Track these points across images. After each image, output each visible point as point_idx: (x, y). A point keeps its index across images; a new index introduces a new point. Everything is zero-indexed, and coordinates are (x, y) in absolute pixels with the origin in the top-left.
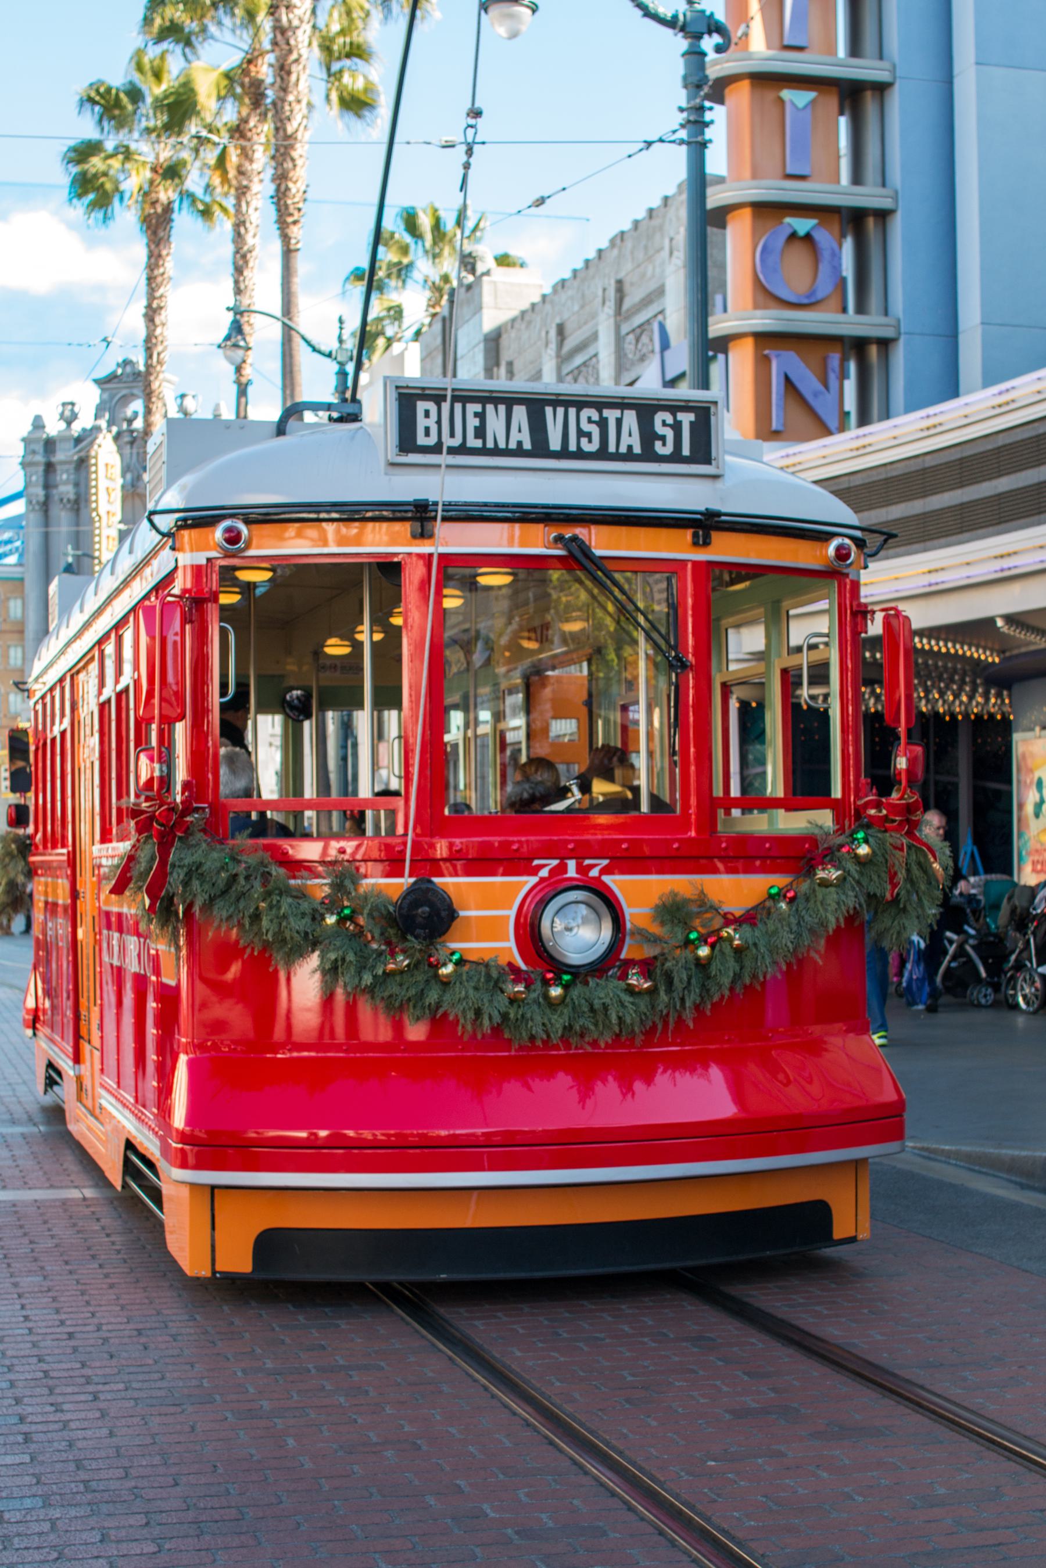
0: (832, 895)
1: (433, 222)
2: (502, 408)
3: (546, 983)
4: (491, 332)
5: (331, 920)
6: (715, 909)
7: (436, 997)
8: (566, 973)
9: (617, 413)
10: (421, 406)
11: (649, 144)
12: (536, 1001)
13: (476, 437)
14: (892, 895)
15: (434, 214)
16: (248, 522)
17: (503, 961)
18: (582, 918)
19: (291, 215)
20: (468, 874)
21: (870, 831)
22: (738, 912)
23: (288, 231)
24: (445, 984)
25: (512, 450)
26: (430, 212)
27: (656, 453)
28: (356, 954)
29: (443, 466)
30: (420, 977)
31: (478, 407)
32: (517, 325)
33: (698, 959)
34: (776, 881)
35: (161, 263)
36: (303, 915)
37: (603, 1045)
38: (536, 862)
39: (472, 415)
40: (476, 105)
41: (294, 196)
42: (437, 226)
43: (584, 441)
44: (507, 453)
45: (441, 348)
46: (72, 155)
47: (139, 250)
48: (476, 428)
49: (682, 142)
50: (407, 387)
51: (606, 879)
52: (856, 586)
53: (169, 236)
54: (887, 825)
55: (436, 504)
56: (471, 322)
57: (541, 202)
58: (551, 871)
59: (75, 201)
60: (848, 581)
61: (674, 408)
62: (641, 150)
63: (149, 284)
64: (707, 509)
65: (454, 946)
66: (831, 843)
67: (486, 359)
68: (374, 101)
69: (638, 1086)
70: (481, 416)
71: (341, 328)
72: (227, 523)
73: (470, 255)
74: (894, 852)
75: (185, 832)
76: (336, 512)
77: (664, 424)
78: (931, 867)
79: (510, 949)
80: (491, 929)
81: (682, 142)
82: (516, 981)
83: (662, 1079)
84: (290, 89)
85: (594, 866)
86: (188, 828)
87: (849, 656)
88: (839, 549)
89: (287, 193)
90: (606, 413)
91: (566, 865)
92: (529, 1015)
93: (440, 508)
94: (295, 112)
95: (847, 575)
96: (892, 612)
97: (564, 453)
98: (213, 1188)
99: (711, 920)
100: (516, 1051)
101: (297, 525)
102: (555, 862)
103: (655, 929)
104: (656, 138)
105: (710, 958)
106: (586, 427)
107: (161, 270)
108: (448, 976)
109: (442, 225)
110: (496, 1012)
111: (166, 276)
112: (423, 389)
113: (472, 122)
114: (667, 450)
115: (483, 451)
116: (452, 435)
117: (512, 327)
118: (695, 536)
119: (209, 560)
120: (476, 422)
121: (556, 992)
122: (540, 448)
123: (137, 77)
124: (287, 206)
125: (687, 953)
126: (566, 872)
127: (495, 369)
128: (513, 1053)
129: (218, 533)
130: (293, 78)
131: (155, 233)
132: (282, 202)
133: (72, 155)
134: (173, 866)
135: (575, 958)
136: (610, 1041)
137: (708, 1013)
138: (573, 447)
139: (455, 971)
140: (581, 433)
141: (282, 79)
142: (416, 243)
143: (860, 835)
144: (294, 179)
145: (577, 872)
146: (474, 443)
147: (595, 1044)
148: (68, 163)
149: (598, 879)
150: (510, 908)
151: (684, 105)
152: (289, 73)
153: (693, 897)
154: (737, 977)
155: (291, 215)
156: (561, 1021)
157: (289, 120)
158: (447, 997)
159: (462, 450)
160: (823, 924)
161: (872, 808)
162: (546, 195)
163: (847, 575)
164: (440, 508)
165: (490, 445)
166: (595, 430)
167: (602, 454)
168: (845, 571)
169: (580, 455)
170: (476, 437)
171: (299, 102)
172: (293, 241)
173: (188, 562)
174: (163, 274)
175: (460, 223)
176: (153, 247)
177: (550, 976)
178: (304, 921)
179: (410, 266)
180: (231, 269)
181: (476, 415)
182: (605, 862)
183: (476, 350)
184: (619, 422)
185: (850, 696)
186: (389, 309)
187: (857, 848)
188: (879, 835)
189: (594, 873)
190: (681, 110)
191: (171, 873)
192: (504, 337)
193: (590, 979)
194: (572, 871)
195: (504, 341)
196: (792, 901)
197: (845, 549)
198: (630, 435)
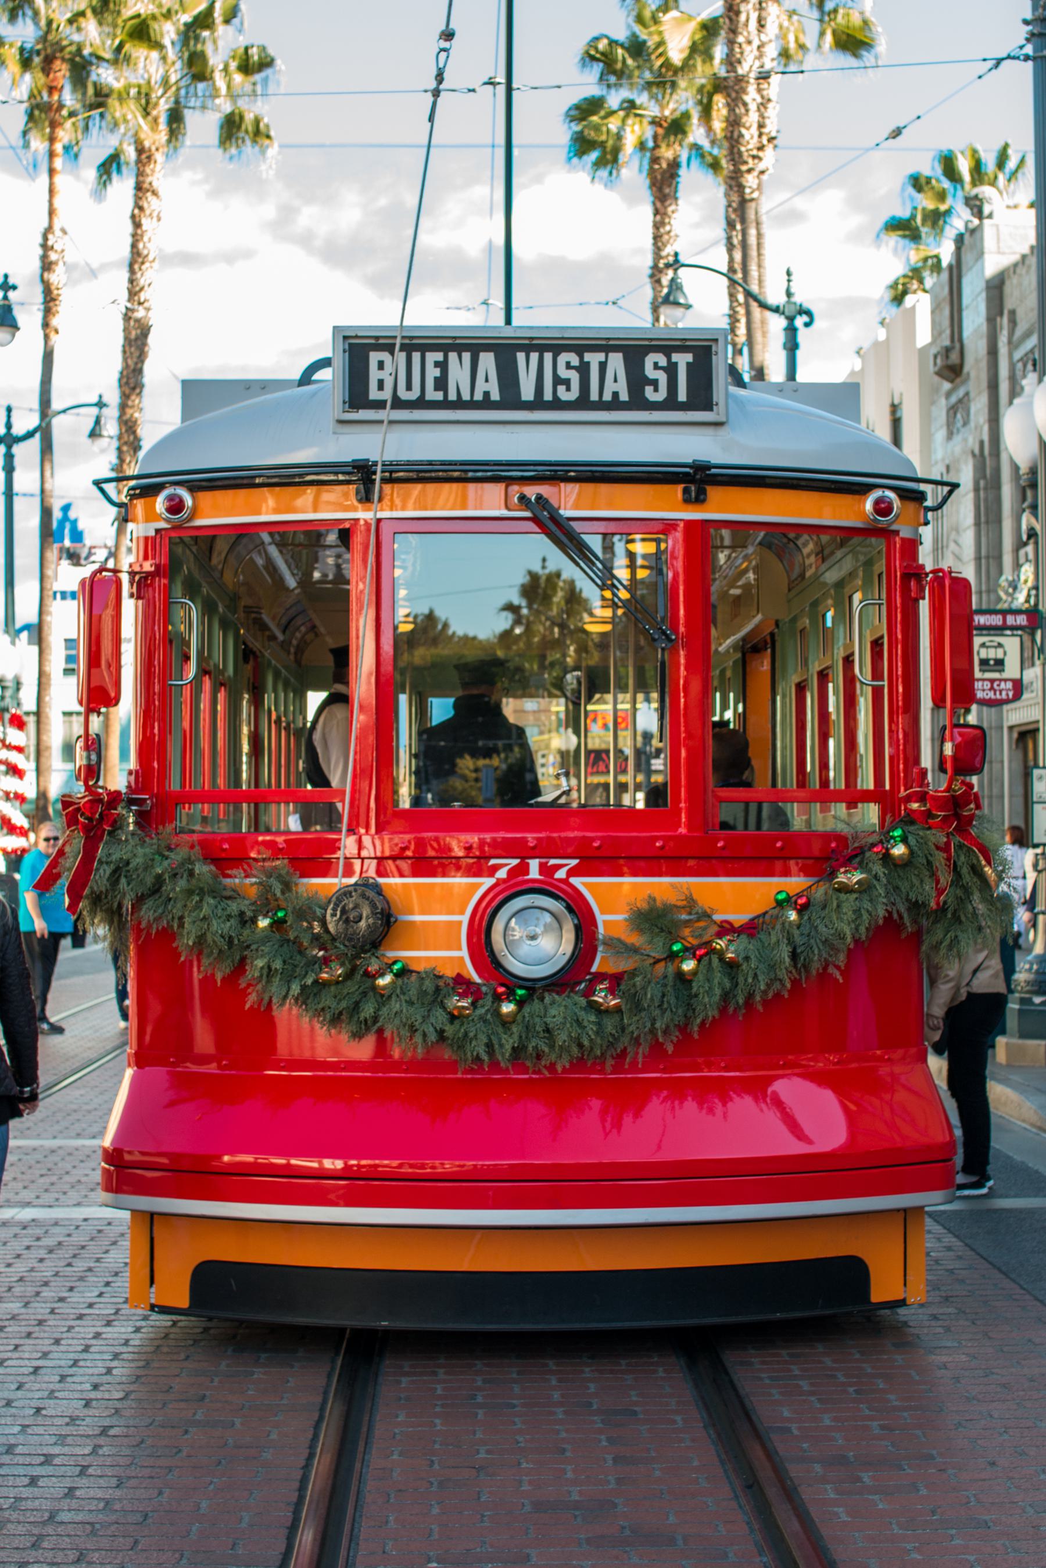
0: (849, 902)
1: (973, 164)
2: (467, 356)
3: (498, 998)
4: (994, 278)
5: (263, 923)
6: (706, 915)
7: (372, 1010)
8: (521, 987)
9: (601, 357)
10: (374, 357)
11: (999, 62)
12: (483, 1019)
13: (436, 389)
14: (938, 903)
15: (973, 156)
16: (194, 488)
17: (450, 973)
18: (545, 926)
19: (746, 163)
20: (415, 874)
21: (912, 828)
22: (739, 918)
23: (743, 181)
24: (383, 997)
25: (477, 402)
26: (969, 153)
27: (647, 400)
28: (284, 962)
29: (386, 422)
30: (351, 987)
31: (439, 356)
32: (1018, 271)
33: (680, 975)
34: (795, 883)
35: (667, 220)
36: (229, 917)
37: (559, 1069)
38: (493, 862)
39: (433, 364)
40: (451, 26)
41: (748, 143)
42: (977, 168)
43: (561, 389)
44: (472, 405)
45: (948, 298)
46: (573, 113)
47: (646, 212)
48: (436, 378)
49: (1027, 58)
50: (357, 337)
51: (575, 881)
52: (912, 546)
53: (676, 192)
54: (930, 821)
55: (375, 464)
56: (974, 269)
57: (897, 133)
58: (509, 872)
59: (575, 160)
60: (897, 539)
61: (668, 348)
62: (990, 70)
63: (655, 244)
64: (694, 461)
65: (391, 954)
66: (863, 842)
67: (988, 308)
68: (872, 39)
69: (628, 1120)
70: (443, 365)
71: (789, 281)
72: (877, 493)
73: (976, 197)
74: (937, 852)
75: (112, 825)
76: (343, 473)
77: (656, 366)
78: (982, 870)
79: (462, 958)
80: (446, 936)
81: (1027, 58)
82: (463, 996)
83: (655, 1108)
84: (740, 30)
85: (559, 867)
86: (115, 821)
87: (899, 626)
88: (877, 502)
89: (741, 140)
90: (588, 357)
91: (528, 864)
92: (471, 1035)
93: (379, 468)
94: (746, 54)
95: (897, 532)
96: (941, 574)
97: (539, 403)
98: (152, 1215)
99: (705, 929)
100: (463, 1073)
101: (314, 488)
102: (515, 862)
103: (634, 939)
104: (1005, 55)
105: (695, 973)
106: (563, 373)
107: (668, 228)
108: (384, 987)
109: (983, 167)
110: (431, 1029)
111: (672, 234)
112: (377, 338)
113: (446, 45)
114: (661, 395)
115: (445, 404)
116: (409, 388)
117: (1014, 272)
118: (686, 491)
119: (157, 531)
120: (437, 372)
121: (508, 1008)
122: (511, 399)
123: (638, 29)
124: (740, 153)
125: (671, 969)
126: (527, 873)
127: (998, 319)
128: (459, 1075)
129: (160, 503)
130: (743, 18)
131: (660, 189)
132: (735, 150)
133: (573, 113)
134: (100, 862)
135: (515, 967)
136: (567, 1065)
137: (696, 1036)
138: (548, 396)
139: (393, 982)
140: (557, 381)
141: (731, 20)
142: (955, 189)
143: (897, 833)
144: (747, 125)
145: (541, 874)
146: (433, 395)
147: (552, 1067)
148: (571, 121)
149: (565, 881)
150: (462, 912)
151: (1029, 16)
152: (738, 13)
153: (680, 903)
154: (726, 996)
155: (746, 163)
156: (511, 1041)
157: (739, 62)
158: (384, 1011)
159: (421, 403)
160: (842, 937)
161: (916, 802)
162: (902, 125)
163: (897, 532)
164: (379, 468)
165: (452, 396)
166: (574, 377)
167: (583, 402)
168: (894, 527)
169: (557, 404)
170: (436, 389)
171: (749, 42)
172: (747, 191)
173: (142, 534)
174: (669, 232)
175: (1001, 163)
176: (659, 205)
177: (501, 990)
178: (228, 924)
179: (948, 212)
180: (723, 224)
181: (437, 364)
182: (574, 862)
183: (979, 299)
184: (603, 366)
185: (900, 672)
186: (925, 260)
187: (893, 847)
188: (921, 833)
189: (561, 874)
190: (1026, 22)
191: (98, 869)
192: (1007, 283)
193: (546, 994)
194: (534, 872)
195: (1007, 289)
196: (801, 910)
197: (884, 502)
198: (616, 381)
